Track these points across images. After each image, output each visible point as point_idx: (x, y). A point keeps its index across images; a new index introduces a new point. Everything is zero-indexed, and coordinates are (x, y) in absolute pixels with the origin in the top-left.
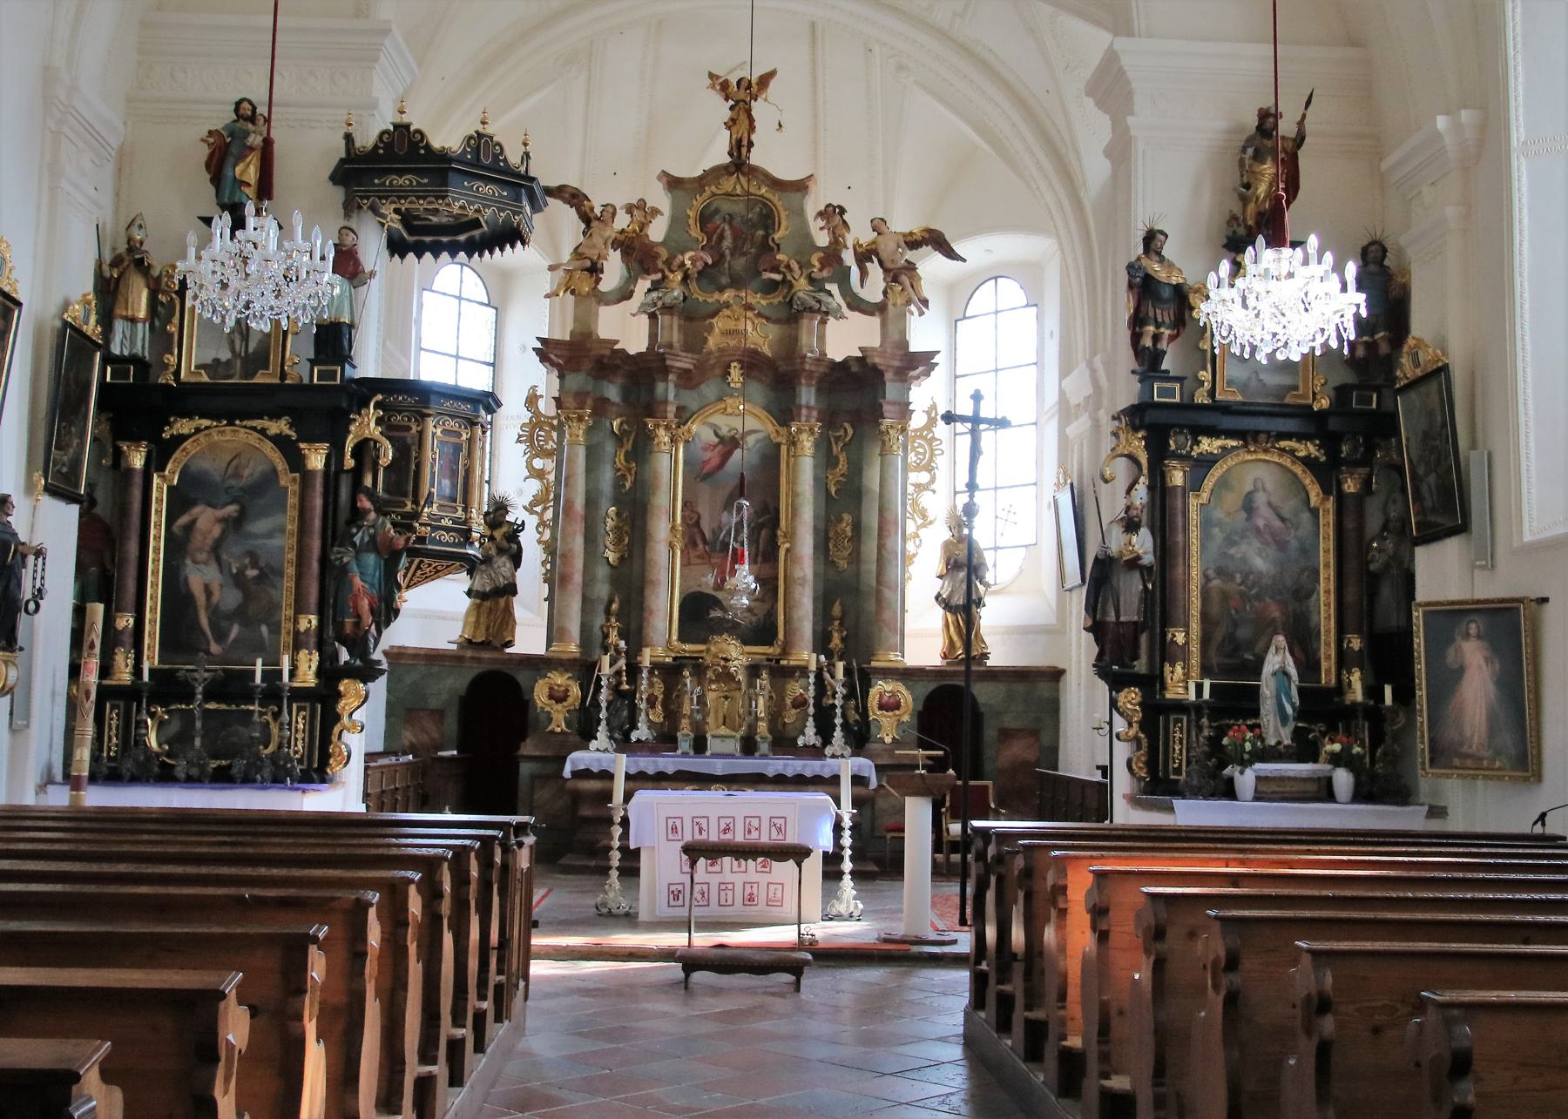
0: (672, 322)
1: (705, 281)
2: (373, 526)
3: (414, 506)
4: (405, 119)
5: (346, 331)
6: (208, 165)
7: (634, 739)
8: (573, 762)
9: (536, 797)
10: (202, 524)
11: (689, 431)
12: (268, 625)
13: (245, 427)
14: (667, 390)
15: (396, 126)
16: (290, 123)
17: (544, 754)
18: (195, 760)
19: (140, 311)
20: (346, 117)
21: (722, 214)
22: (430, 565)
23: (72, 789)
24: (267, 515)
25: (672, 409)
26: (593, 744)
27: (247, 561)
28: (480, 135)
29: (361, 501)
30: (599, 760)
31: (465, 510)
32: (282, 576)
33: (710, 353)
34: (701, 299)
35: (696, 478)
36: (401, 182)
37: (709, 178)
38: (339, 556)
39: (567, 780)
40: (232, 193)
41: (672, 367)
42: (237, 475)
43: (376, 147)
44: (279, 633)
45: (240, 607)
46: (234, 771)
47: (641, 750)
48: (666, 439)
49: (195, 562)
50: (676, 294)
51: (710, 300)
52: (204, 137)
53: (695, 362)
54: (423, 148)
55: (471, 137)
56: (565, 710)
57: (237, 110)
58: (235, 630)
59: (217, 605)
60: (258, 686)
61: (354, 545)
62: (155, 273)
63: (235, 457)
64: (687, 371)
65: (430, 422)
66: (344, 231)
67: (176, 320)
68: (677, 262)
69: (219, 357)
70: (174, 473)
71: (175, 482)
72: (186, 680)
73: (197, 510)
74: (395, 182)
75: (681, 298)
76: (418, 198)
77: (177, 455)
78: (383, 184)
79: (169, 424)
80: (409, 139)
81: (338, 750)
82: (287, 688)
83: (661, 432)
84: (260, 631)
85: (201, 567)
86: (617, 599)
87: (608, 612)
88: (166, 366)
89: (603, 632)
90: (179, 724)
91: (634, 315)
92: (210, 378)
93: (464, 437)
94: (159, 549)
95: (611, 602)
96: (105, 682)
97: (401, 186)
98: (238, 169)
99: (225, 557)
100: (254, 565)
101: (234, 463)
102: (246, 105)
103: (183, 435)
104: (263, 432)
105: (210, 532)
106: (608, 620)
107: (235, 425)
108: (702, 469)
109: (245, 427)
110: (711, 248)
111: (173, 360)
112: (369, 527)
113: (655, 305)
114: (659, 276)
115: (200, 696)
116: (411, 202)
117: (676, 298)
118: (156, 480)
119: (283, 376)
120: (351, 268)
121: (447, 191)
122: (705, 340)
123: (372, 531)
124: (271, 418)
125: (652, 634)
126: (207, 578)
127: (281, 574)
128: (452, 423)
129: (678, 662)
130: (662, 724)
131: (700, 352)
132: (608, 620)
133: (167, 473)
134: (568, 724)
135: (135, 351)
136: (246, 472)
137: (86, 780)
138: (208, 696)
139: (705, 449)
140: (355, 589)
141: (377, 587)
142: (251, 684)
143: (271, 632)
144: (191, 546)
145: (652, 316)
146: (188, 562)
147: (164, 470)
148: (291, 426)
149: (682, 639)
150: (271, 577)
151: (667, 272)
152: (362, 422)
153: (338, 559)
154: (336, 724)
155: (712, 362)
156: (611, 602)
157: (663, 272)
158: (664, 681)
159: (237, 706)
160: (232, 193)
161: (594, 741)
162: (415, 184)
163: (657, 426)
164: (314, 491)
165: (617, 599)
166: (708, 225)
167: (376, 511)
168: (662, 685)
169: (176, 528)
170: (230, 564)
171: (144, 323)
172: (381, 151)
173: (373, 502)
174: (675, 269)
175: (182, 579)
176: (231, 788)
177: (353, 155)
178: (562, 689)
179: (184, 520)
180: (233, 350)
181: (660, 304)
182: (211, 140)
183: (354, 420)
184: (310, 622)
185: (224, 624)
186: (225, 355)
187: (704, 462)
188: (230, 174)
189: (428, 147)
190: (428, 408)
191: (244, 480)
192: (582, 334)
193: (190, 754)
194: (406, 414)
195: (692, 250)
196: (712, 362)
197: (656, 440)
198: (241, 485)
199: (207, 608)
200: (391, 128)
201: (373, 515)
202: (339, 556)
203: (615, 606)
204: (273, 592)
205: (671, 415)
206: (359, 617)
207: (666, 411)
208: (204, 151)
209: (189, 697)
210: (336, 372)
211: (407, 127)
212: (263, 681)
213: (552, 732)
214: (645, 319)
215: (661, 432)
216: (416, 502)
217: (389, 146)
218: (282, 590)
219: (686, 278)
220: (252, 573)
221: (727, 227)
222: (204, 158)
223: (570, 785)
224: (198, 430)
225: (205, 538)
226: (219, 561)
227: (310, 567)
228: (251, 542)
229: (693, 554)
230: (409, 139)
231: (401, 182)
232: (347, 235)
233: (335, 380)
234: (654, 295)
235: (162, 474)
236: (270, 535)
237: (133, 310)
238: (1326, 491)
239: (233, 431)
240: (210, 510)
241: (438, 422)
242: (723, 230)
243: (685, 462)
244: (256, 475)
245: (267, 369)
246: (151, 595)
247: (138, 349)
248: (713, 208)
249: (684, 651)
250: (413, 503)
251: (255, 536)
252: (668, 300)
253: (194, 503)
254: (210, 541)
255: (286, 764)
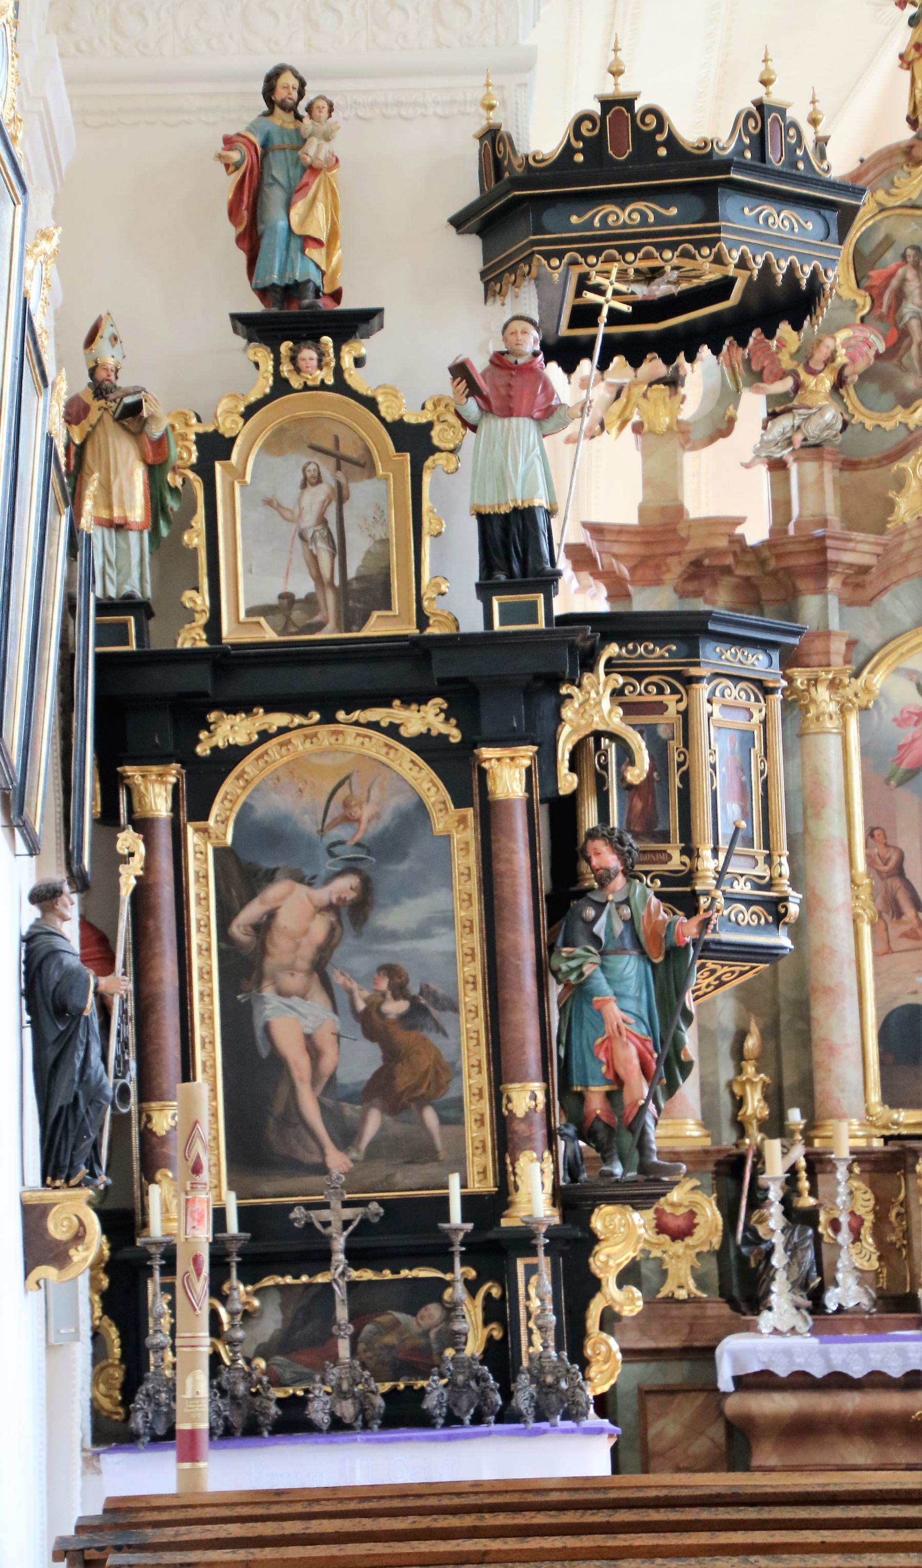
0: (822, 474)
1: (872, 388)
2: (627, 902)
3: (686, 859)
4: (625, 87)
5: (541, 519)
6: (233, 212)
7: (832, 1306)
8: (735, 1358)
9: (652, 1432)
10: (284, 919)
11: (867, 689)
12: (438, 1109)
13: (357, 723)
14: (825, 607)
15: (607, 104)
16: (361, 113)
17: (662, 1345)
18: (345, 1386)
19: (132, 508)
20: (484, 92)
21: (899, 248)
22: (713, 972)
23: (181, 1459)
24: (414, 894)
25: (838, 646)
26: (766, 1320)
27: (384, 984)
28: (760, 106)
29: (598, 854)
30: (788, 1353)
31: (769, 860)
32: (456, 1010)
33: (903, 529)
34: (869, 424)
35: (887, 781)
36: (624, 216)
37: (871, 175)
38: (573, 964)
39: (726, 1395)
40: (287, 261)
41: (837, 563)
42: (348, 819)
43: (568, 151)
44: (459, 1121)
45: (377, 1075)
46: (430, 1402)
47: (850, 1326)
48: (832, 708)
49: (280, 993)
50: (829, 416)
51: (888, 425)
52: (220, 151)
53: (879, 550)
54: (664, 144)
55: (749, 115)
56: (693, 1253)
57: (269, 92)
58: (374, 1122)
59: (333, 1078)
60: (456, 1230)
61: (595, 940)
62: (156, 432)
63: (340, 785)
64: (864, 570)
65: (703, 690)
66: (518, 326)
67: (199, 521)
68: (822, 353)
69: (291, 589)
70: (225, 821)
71: (229, 840)
72: (309, 1225)
73: (274, 892)
74: (611, 219)
75: (839, 426)
76: (660, 247)
77: (228, 786)
78: (589, 225)
79: (207, 726)
80: (635, 128)
81: (603, 1348)
82: (543, 1229)
83: (822, 693)
84: (422, 1122)
85: (295, 1001)
86: (754, 1029)
87: (738, 1055)
88: (189, 615)
89: (733, 1095)
90: (279, 1316)
91: (747, 466)
92: (280, 633)
93: (757, 717)
94: (210, 973)
95: (741, 1036)
96: (219, 1235)
97: (625, 225)
98: (296, 213)
99: (338, 979)
100: (399, 991)
101: (343, 792)
102: (288, 80)
103: (236, 746)
104: (393, 731)
105: (306, 932)
106: (740, 1070)
107: (336, 722)
108: (900, 760)
109: (357, 723)
110: (881, 318)
111: (202, 600)
112: (619, 904)
113: (790, 442)
114: (787, 384)
115: (341, 1257)
116: (648, 256)
117: (829, 426)
118: (192, 838)
119: (422, 620)
120: (540, 398)
121: (717, 230)
122: (891, 506)
123: (626, 911)
124: (406, 703)
125: (838, 1094)
126: (308, 1026)
127: (453, 1007)
128: (735, 692)
129: (892, 1147)
130: (877, 1273)
131: (881, 531)
132: (740, 1070)
133: (211, 822)
134: (701, 1283)
135: (127, 589)
136: (366, 812)
137: (205, 1437)
138: (356, 1258)
139: (901, 722)
140: (610, 1029)
141: (646, 1020)
142: (445, 1226)
143: (443, 1121)
144: (269, 964)
145: (777, 466)
146: (268, 992)
147: (206, 818)
148: (448, 714)
149: (892, 1098)
150: (434, 1012)
151: (803, 376)
152: (587, 700)
153: (572, 970)
154: (592, 1296)
155: (905, 548)
156: (741, 1036)
157: (795, 374)
158: (872, 1186)
159: (393, 1272)
160: (287, 261)
161: (766, 1314)
162: (651, 219)
163: (815, 681)
164: (511, 836)
165: (754, 1029)
166: (872, 273)
167: (624, 873)
168: (869, 1195)
169: (239, 928)
170: (350, 992)
171: (141, 532)
172: (579, 158)
173: (621, 855)
174: (820, 367)
175: (258, 1024)
176: (260, 1446)
177: (775, 159)
178: (682, 1211)
179: (252, 911)
180: (318, 578)
181: (798, 439)
182: (235, 156)
183: (570, 696)
184: (534, 1097)
185: (350, 1110)
186: (302, 586)
187: (900, 747)
188: (282, 224)
189: (672, 142)
190: (697, 664)
191: (363, 826)
192: (663, 511)
193: (333, 1374)
194: (654, 679)
195: (847, 326)
196: (905, 548)
197: (813, 711)
198: (358, 838)
199: (314, 1081)
200: (596, 108)
201: (619, 881)
202: (573, 964)
203: (752, 1043)
204: (434, 1038)
205: (837, 660)
206: (619, 1081)
207: (827, 653)
208: (227, 184)
209: (323, 1260)
210: (534, 604)
211: (629, 103)
212: (241, 1228)
213: (671, 1300)
214: (762, 474)
215: (822, 693)
216: (690, 851)
217: (595, 147)
218: (458, 1036)
219: (840, 383)
220: (395, 1008)
221: (911, 274)
222: (228, 194)
223: (735, 1405)
224: (265, 736)
225: (298, 946)
226: (327, 985)
227: (521, 989)
228: (388, 947)
229: (895, 930)
230: (635, 128)
231: (624, 216)
232: (524, 332)
233: (535, 621)
234: (785, 423)
235: (200, 824)
236: (423, 932)
237: (122, 505)
238: (461, 800)
239: (334, 732)
240: (301, 890)
241: (713, 693)
242: (904, 280)
243: (865, 752)
244: (387, 818)
245: (388, 607)
246: (204, 1064)
247: (132, 586)
248: (880, 236)
249: (896, 1123)
250: (683, 852)
251: (394, 936)
252: (813, 430)
253: (270, 877)
254: (307, 952)
255: (558, 1380)
